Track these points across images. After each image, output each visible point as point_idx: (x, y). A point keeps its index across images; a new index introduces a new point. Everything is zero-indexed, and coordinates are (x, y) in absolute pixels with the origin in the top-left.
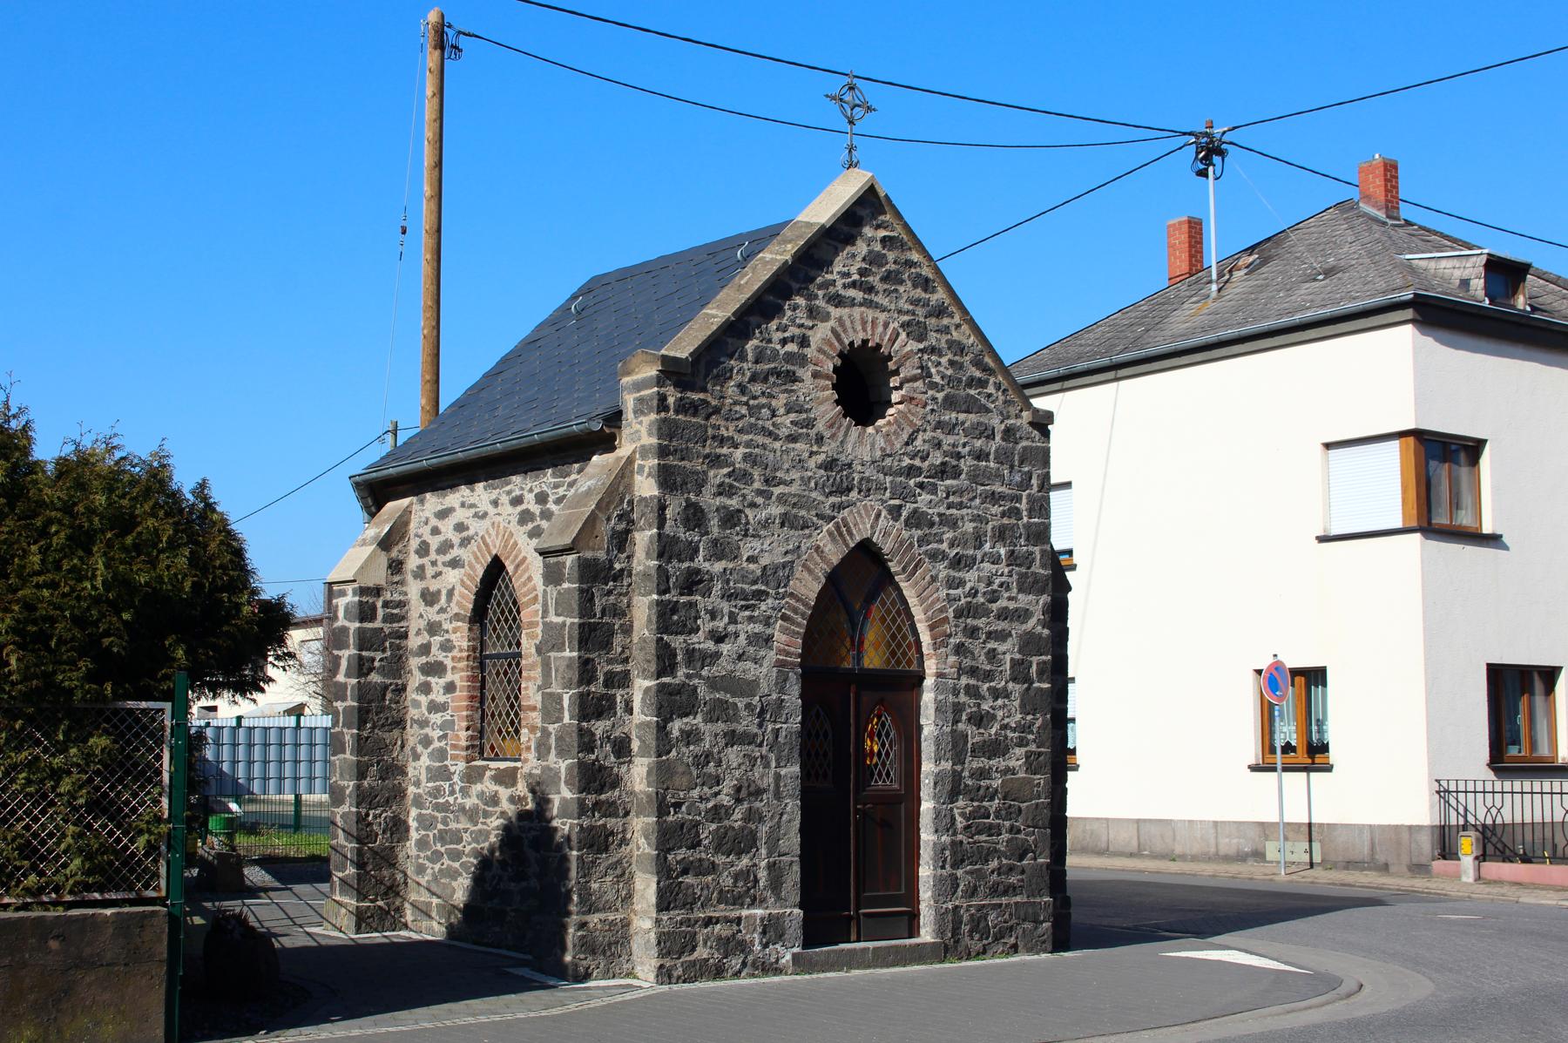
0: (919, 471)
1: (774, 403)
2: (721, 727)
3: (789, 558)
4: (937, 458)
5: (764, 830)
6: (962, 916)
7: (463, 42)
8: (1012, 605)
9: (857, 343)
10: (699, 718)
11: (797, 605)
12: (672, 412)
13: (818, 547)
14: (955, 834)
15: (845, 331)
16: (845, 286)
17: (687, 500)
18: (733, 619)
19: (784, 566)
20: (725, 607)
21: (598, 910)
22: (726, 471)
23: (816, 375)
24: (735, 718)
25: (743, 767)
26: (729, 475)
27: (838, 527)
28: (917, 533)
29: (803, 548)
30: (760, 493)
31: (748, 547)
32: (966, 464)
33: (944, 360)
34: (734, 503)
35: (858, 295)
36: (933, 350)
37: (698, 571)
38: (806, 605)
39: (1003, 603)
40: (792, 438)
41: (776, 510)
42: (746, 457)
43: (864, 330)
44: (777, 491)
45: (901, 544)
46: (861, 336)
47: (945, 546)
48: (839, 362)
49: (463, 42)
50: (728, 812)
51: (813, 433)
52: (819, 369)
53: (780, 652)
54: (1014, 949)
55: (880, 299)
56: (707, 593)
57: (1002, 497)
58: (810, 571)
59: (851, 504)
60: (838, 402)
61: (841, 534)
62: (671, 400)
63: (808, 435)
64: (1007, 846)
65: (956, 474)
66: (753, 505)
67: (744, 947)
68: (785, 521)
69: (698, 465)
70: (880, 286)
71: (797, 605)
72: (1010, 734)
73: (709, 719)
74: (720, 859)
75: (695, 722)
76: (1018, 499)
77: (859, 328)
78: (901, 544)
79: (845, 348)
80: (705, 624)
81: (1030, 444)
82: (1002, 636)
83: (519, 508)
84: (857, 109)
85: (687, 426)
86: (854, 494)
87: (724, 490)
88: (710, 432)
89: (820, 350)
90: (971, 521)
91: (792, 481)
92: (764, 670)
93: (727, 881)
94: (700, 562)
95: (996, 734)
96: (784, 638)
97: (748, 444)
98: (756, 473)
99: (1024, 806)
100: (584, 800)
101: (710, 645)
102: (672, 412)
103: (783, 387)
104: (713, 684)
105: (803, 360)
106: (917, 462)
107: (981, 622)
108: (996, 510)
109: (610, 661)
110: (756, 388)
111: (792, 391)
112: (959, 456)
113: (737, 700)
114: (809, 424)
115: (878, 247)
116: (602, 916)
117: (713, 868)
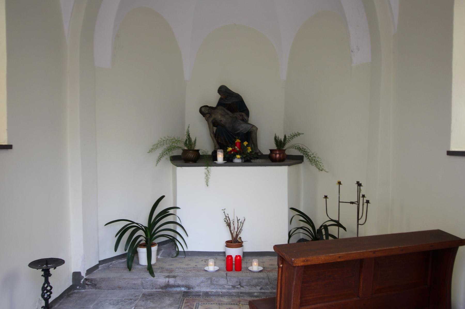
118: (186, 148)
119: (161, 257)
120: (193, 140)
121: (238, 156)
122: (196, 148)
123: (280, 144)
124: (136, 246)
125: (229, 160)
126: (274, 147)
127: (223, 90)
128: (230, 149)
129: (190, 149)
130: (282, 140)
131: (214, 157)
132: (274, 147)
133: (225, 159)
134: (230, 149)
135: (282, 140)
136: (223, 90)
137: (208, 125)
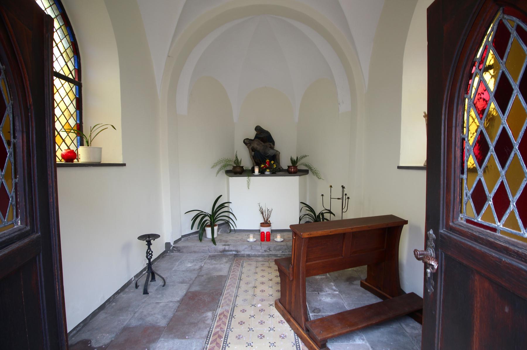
120: (239, 160)
122: (241, 165)
123: (294, 162)
125: (262, 173)
127: (258, 129)
130: (296, 160)
131: (253, 171)
135: (296, 160)
136: (258, 129)
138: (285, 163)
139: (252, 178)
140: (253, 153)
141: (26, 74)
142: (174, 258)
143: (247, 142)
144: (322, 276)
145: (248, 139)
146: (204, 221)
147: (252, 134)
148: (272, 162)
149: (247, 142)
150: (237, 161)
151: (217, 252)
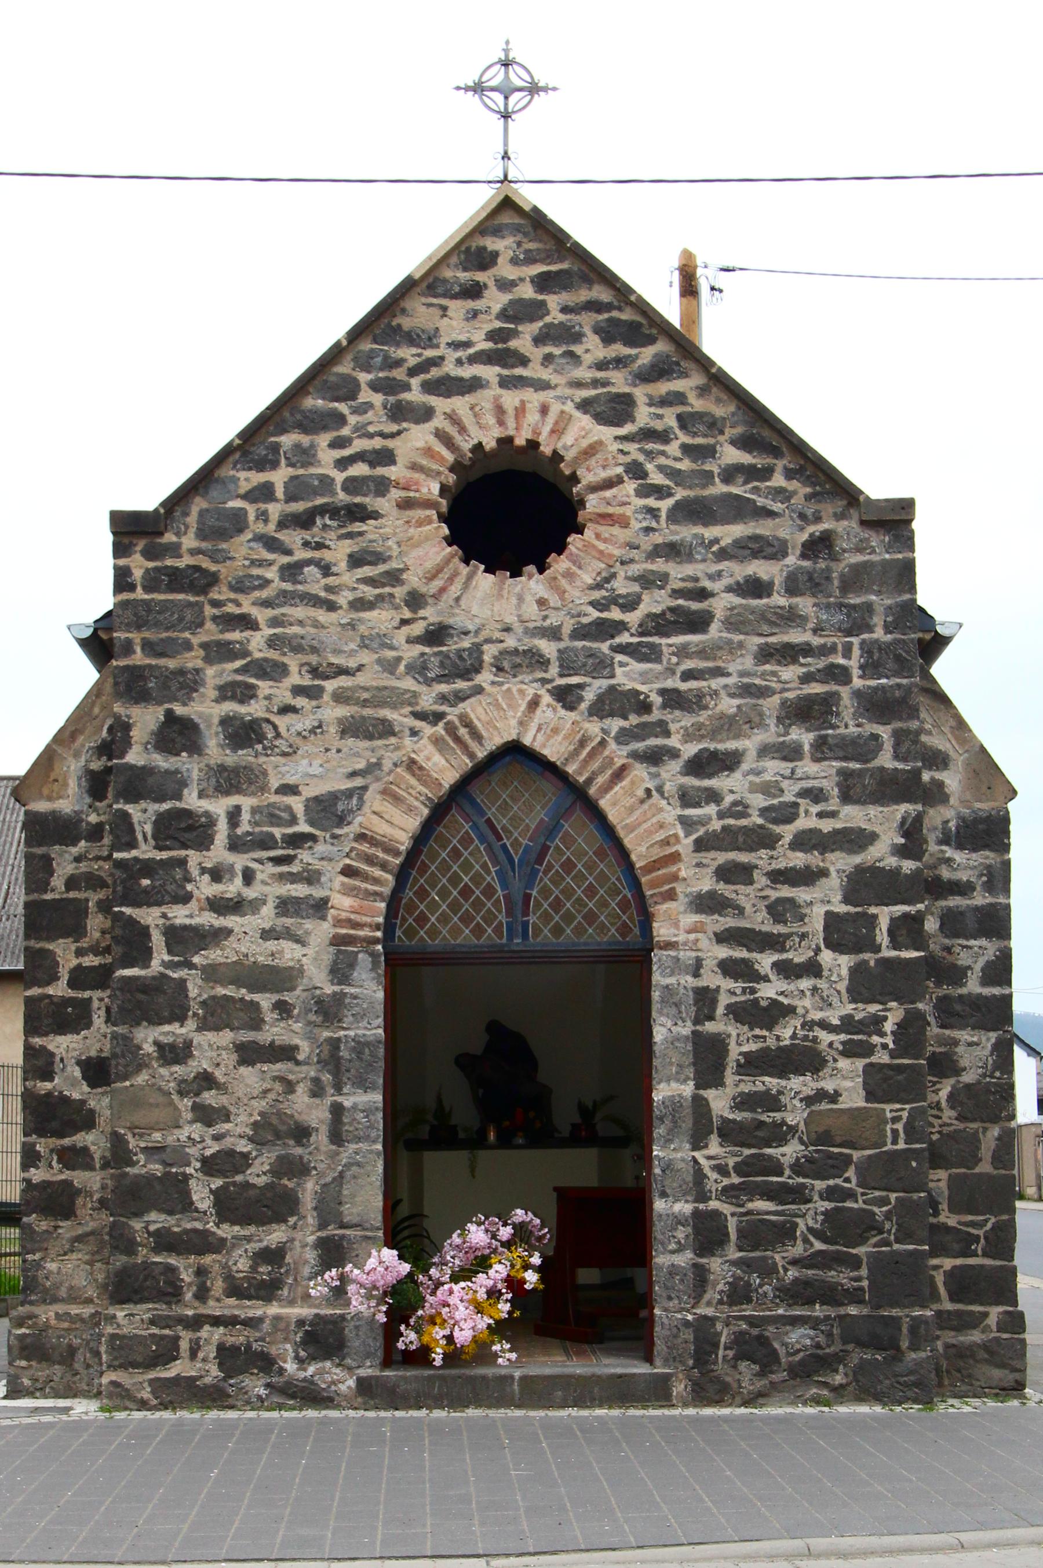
0: (621, 626)
1: (327, 555)
2: (227, 1037)
3: (358, 782)
4: (655, 602)
5: (309, 1190)
6: (720, 1334)
7: (723, 280)
8: (826, 826)
9: (490, 444)
10: (191, 1024)
11: (372, 851)
12: (139, 589)
13: (413, 762)
14: (702, 1196)
15: (463, 430)
16: (459, 362)
17: (169, 713)
18: (248, 877)
19: (349, 794)
20: (240, 861)
21: (55, 1300)
22: (238, 664)
23: (406, 505)
24: (257, 1024)
25: (271, 1096)
26: (243, 670)
27: (451, 729)
28: (616, 724)
29: (387, 765)
30: (298, 691)
31: (293, 771)
32: (722, 604)
33: (673, 448)
34: (254, 709)
35: (490, 373)
36: (648, 434)
37: (187, 813)
38: (396, 853)
39: (803, 823)
40: (360, 605)
41: (332, 713)
42: (272, 642)
43: (501, 423)
44: (330, 686)
45: (582, 743)
46: (497, 432)
47: (674, 742)
48: (451, 479)
49: (723, 280)
50: (243, 1161)
51: (399, 592)
52: (412, 494)
53: (338, 922)
54: (839, 1394)
55: (534, 371)
56: (204, 842)
57: (806, 650)
58: (397, 799)
59: (479, 690)
60: (450, 541)
61: (458, 739)
62: (138, 574)
63: (392, 596)
64: (824, 1222)
65: (698, 623)
66: (287, 709)
67: (266, 1363)
68: (350, 729)
69: (193, 660)
70: (536, 353)
71: (372, 851)
72: (825, 1037)
73: (204, 1026)
74: (226, 1231)
75: (183, 1030)
76: (847, 653)
77: (491, 420)
78: (582, 743)
79: (463, 456)
80: (205, 888)
81: (867, 558)
82: (808, 877)
83: (654, 793)
84: (517, 95)
85: (165, 606)
86: (484, 678)
87: (230, 692)
88: (209, 611)
89: (414, 467)
90: (732, 696)
91: (360, 668)
92: (310, 951)
93: (242, 1264)
94: (191, 800)
95: (794, 1036)
96: (347, 902)
97: (275, 622)
98: (292, 662)
99: (856, 1155)
100: (34, 1145)
101: (208, 919)
102: (139, 589)
103: (344, 531)
104: (212, 973)
105: (382, 486)
106: (615, 614)
107: (760, 858)
108: (790, 673)
109: (80, 953)
110: (293, 538)
111: (361, 534)
112: (703, 594)
113: (256, 997)
114: (394, 577)
115: (527, 292)
116: (60, 1308)
117: (216, 1246)
118: (435, 1123)
119: (740, 1249)
120: (447, 1109)
121: (521, 1134)
122: (453, 1122)
123: (587, 1113)
124: (994, 1258)
125: (505, 1142)
126: (577, 1119)
127: (494, 1028)
128: (507, 1123)
129: (592, 791)
130: (590, 1108)
131: (483, 1134)
132: (577, 1119)
133: (498, 1137)
134: (507, 1123)
135: (590, 1108)
136: (494, 1028)
137: (814, 452)
138: (565, 1117)
139: (482, 1154)
140: (481, 1091)
141: (242, 1233)
142: (713, 1162)
143: (465, 1062)
144: (397, 1370)
145: (467, 1055)
146: (521, 377)
147: (477, 1043)
148: (532, 1114)
149: (465, 1062)
150: (441, 1113)
151: (702, 1500)
